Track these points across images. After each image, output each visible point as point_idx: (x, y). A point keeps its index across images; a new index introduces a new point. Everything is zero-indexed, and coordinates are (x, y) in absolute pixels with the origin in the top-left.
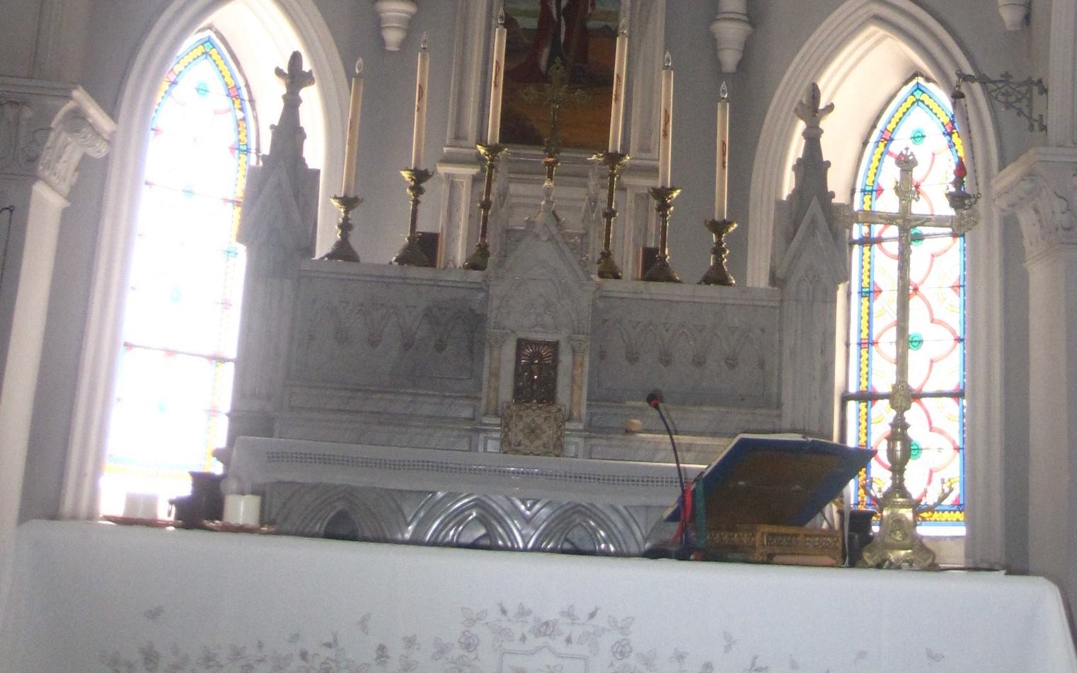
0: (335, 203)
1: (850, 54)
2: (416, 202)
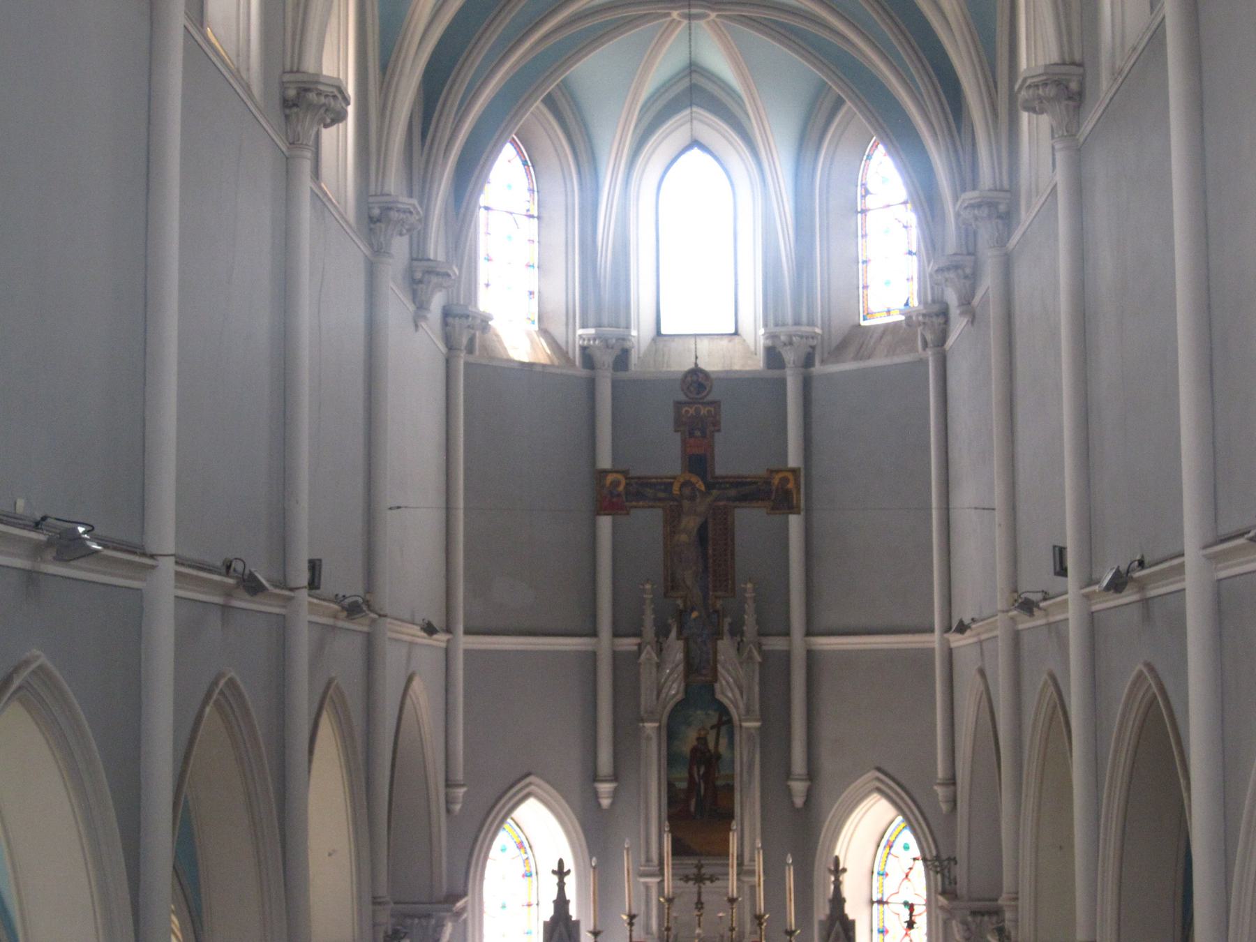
0: (589, 935)
1: (865, 806)
2: (631, 931)
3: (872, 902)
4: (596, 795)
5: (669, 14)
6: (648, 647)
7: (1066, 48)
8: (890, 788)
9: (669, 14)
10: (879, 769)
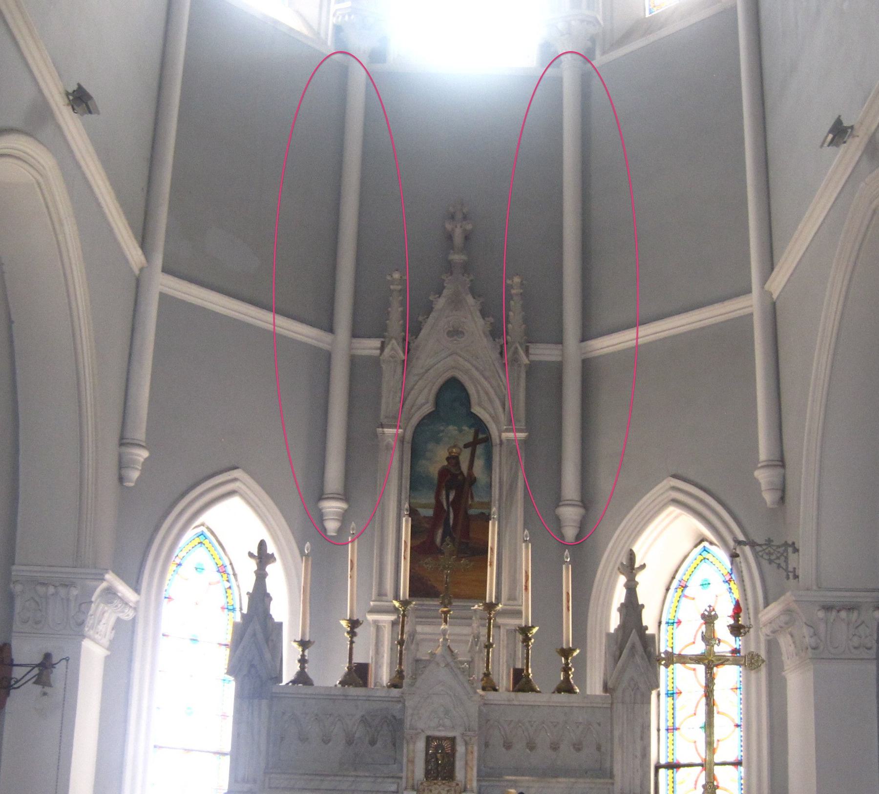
0: (295, 645)
2: (352, 642)
4: (321, 516)
6: (394, 341)
10: (675, 476)
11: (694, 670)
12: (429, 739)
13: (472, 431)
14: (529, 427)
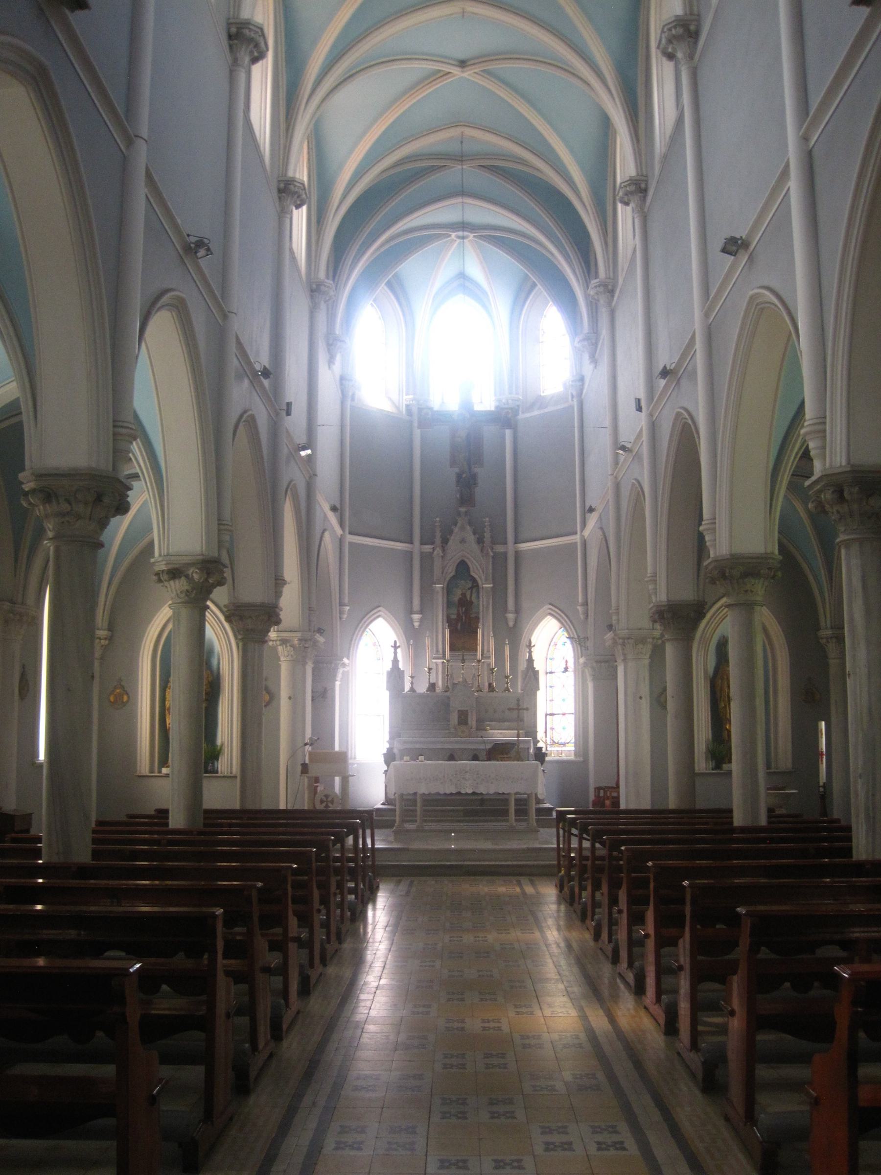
2: (429, 676)
3: (547, 673)
5: (450, 236)
6: (438, 549)
7: (639, 170)
8: (557, 613)
9: (450, 236)
10: (550, 604)
11: (566, 669)
12: (459, 711)
13: (471, 582)
14: (494, 583)
